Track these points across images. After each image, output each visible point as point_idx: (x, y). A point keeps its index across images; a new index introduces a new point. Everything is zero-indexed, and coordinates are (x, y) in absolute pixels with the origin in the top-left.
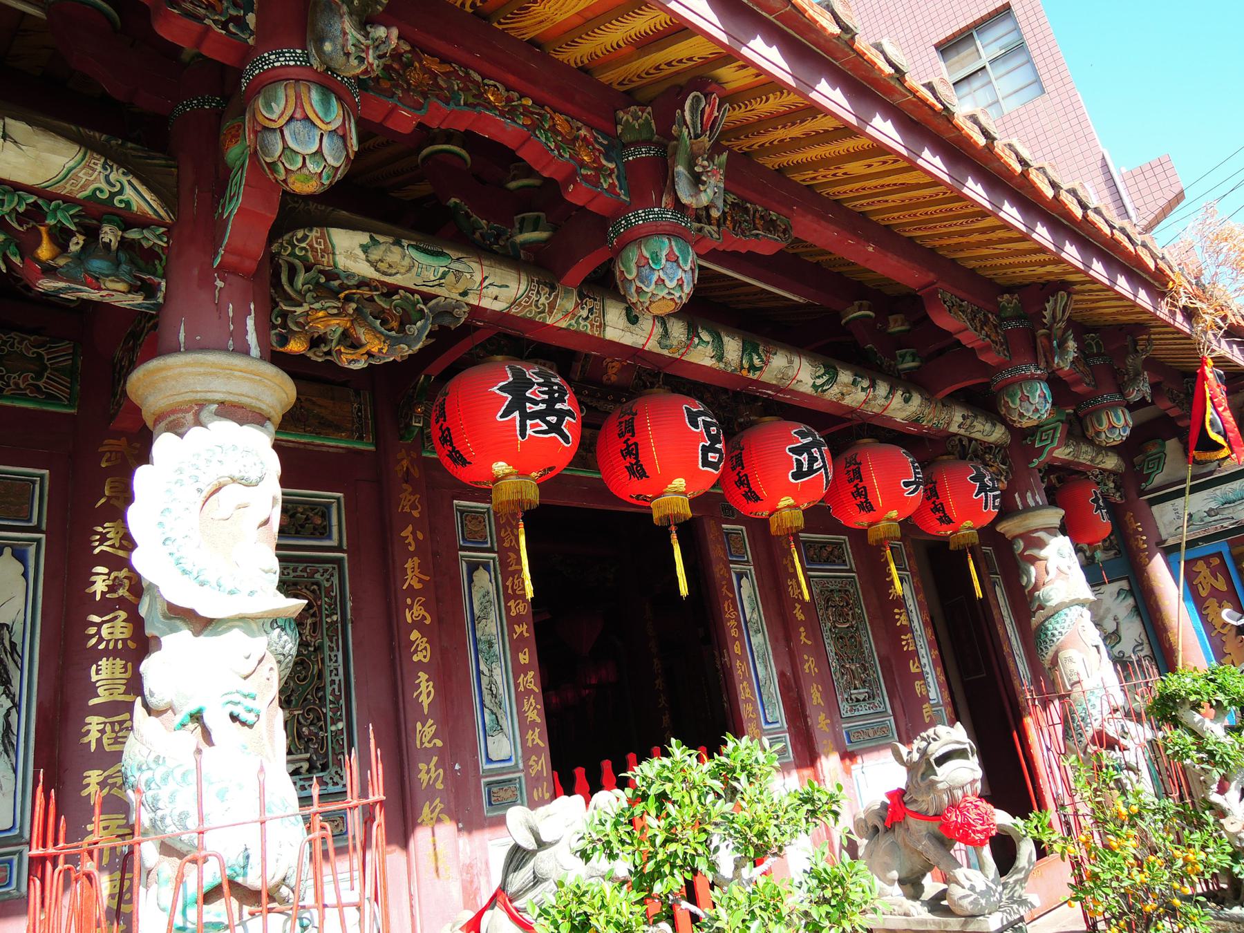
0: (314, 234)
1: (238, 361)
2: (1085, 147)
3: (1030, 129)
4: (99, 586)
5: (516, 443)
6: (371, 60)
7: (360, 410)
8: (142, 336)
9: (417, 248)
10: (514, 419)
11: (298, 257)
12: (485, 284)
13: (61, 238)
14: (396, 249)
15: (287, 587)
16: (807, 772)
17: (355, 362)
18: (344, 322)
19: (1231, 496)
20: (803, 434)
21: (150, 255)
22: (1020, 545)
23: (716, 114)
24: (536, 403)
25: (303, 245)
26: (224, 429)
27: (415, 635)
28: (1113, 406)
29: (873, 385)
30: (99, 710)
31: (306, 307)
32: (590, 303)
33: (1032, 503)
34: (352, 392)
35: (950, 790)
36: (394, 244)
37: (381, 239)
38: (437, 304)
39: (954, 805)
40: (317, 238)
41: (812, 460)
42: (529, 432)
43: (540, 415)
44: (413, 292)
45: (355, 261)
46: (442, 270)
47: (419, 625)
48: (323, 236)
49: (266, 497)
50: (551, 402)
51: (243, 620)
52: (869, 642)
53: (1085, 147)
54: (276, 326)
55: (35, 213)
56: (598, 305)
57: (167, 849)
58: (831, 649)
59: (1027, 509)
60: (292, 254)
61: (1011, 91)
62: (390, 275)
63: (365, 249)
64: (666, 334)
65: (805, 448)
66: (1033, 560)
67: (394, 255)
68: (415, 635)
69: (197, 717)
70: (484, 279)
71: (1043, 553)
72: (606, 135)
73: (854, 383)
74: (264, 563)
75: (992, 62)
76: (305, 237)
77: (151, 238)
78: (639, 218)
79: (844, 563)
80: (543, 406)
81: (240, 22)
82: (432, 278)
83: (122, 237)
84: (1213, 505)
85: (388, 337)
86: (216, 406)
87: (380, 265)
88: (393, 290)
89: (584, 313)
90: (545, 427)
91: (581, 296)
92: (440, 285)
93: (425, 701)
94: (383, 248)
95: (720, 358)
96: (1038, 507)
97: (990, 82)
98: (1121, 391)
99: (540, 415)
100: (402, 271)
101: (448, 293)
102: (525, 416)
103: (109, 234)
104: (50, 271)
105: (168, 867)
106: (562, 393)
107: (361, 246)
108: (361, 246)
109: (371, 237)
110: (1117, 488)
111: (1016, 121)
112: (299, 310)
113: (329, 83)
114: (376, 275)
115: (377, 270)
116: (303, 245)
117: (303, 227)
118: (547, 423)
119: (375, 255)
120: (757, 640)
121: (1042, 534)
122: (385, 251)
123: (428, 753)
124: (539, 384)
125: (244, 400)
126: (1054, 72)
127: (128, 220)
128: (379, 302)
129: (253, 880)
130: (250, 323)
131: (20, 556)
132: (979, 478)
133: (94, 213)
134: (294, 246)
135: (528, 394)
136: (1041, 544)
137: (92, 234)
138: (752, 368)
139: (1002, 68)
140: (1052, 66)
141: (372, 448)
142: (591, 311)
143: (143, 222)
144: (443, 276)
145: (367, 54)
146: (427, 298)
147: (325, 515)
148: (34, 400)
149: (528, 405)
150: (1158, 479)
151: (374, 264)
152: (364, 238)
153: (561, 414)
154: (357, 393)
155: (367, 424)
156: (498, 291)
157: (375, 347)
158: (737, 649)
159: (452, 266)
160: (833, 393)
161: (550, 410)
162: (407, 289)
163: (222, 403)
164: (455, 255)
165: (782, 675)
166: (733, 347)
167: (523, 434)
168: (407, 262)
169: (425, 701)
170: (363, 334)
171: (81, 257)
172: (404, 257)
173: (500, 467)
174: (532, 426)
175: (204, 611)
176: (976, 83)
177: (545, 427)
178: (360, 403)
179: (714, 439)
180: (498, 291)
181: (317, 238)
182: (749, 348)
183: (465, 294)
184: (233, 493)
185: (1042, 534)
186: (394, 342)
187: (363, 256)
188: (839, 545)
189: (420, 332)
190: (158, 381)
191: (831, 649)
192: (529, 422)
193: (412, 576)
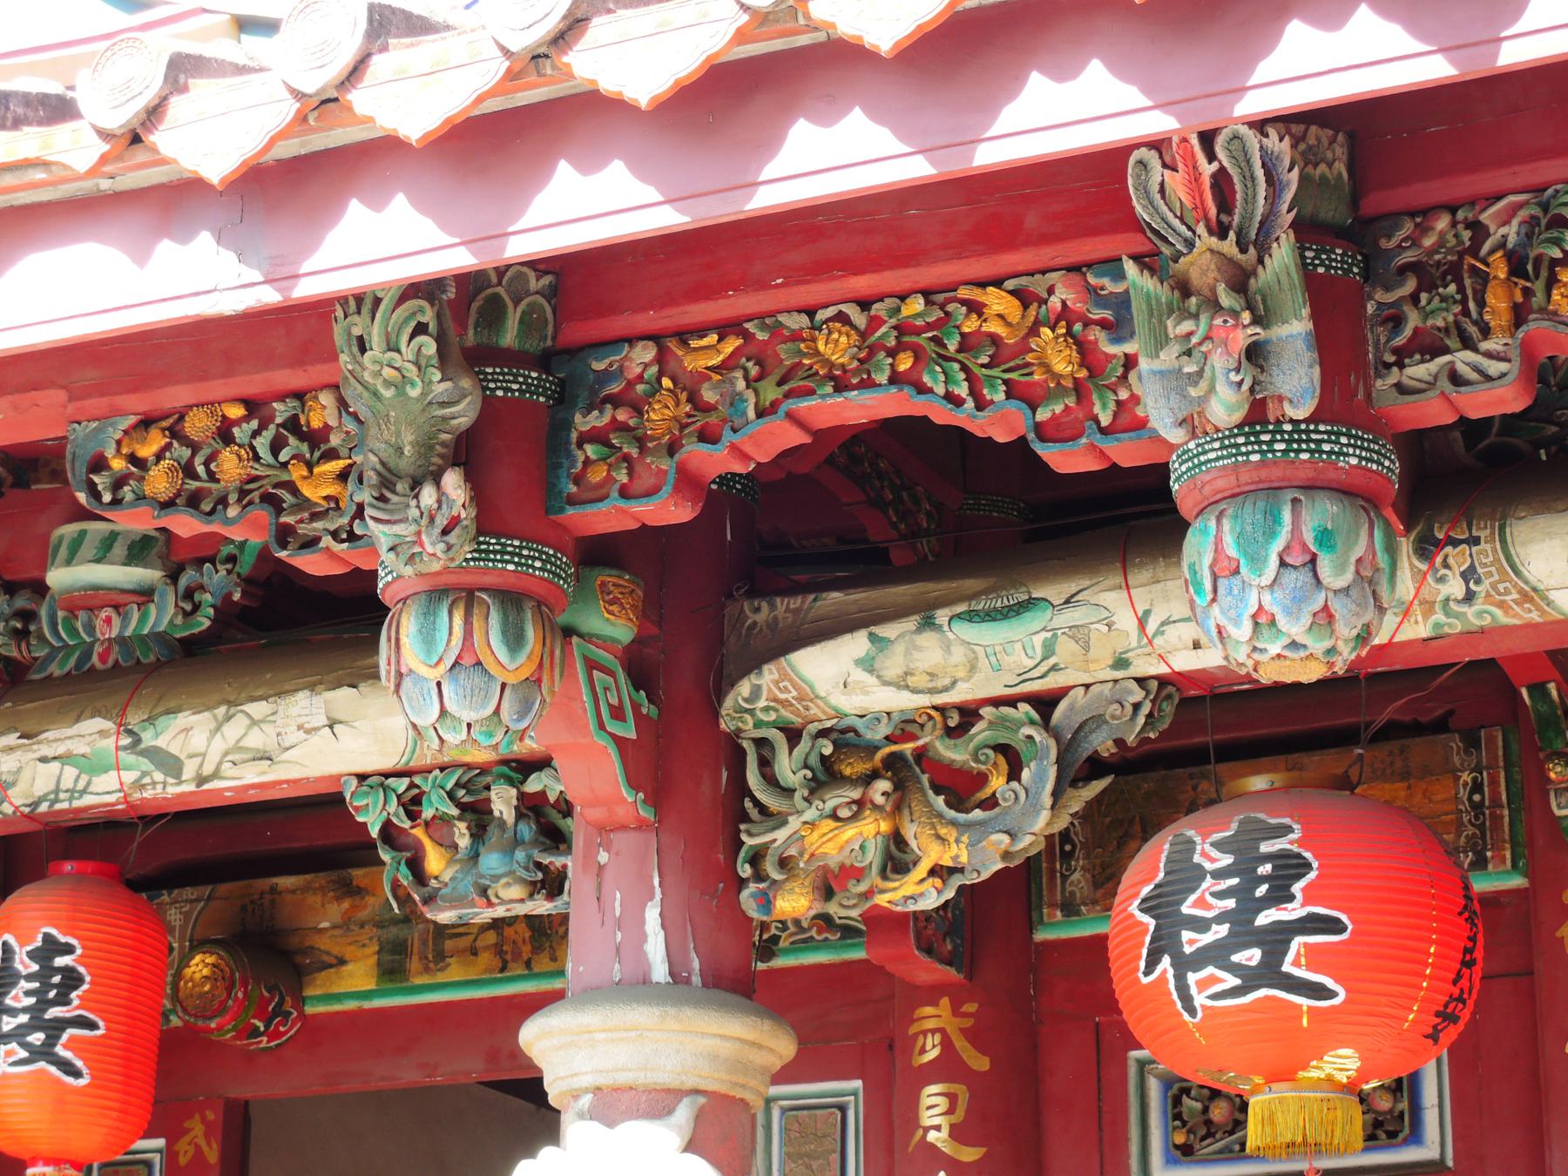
0: (768, 676)
6: (430, 549)
7: (1477, 787)
9: (971, 617)
10: (1162, 979)
11: (768, 724)
12: (1151, 628)
14: (928, 639)
17: (918, 893)
18: (872, 828)
23: (1208, 169)
24: (1201, 925)
25: (762, 703)
31: (794, 823)
32: (1458, 557)
34: (1456, 742)
36: (920, 629)
37: (888, 631)
38: (1071, 708)
40: (776, 683)
42: (1200, 1000)
43: (1216, 954)
44: (1011, 702)
45: (867, 693)
46: (1038, 640)
48: (784, 676)
56: (1486, 552)
60: (758, 724)
62: (946, 689)
63: (868, 664)
70: (1142, 624)
76: (756, 692)
80: (1221, 931)
82: (1030, 663)
83: (522, 796)
85: (969, 826)
86: (590, 1096)
87: (911, 681)
89: (1456, 588)
90: (1232, 981)
91: (1427, 548)
92: (1054, 668)
94: (899, 648)
99: (1216, 954)
100: (961, 674)
102: (1183, 965)
107: (859, 662)
108: (859, 662)
109: (873, 638)
112: (781, 835)
114: (924, 700)
115: (915, 691)
116: (762, 703)
117: (745, 673)
118: (1235, 969)
119: (893, 665)
122: (907, 653)
124: (1219, 875)
125: (623, 1078)
128: (911, 767)
130: (652, 915)
134: (751, 712)
135: (1186, 909)
141: (1517, 881)
142: (1469, 575)
144: (1049, 649)
145: (422, 545)
146: (1045, 703)
148: (825, 945)
149: (1186, 935)
151: (901, 684)
152: (856, 644)
154: (1471, 742)
155: (1496, 820)
157: (953, 853)
159: (1056, 623)
161: (1243, 933)
162: (997, 702)
163: (597, 1090)
164: (1053, 591)
167: (1192, 1011)
168: (958, 655)
172: (947, 647)
174: (1203, 985)
177: (1232, 981)
178: (1478, 769)
181: (776, 683)
183: (1121, 663)
187: (871, 680)
192: (1192, 978)
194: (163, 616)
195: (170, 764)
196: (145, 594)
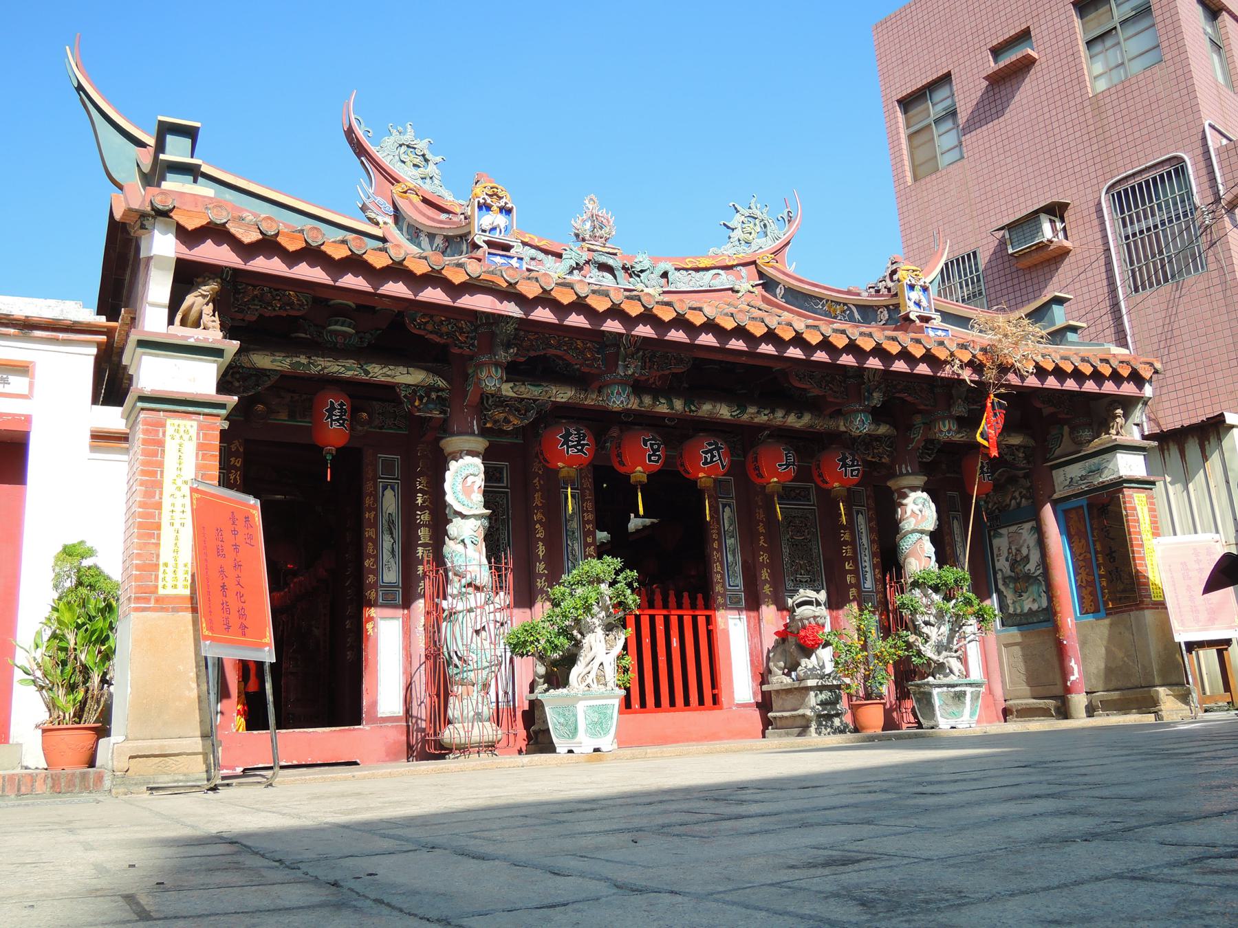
1: (472, 438)
2: (1190, 118)
3: (1145, 96)
4: (420, 501)
5: (569, 452)
8: (445, 429)
13: (421, 399)
15: (486, 507)
16: (753, 614)
19: (1093, 468)
20: (710, 444)
21: (445, 399)
22: (896, 495)
26: (468, 459)
27: (538, 526)
28: (943, 419)
29: (773, 412)
30: (421, 545)
33: (904, 471)
35: (801, 620)
39: (804, 627)
41: (713, 456)
43: (574, 446)
47: (539, 522)
49: (479, 481)
50: (579, 442)
51: (474, 516)
52: (818, 549)
53: (1190, 118)
54: (482, 420)
55: (415, 392)
57: (455, 574)
58: (786, 551)
59: (902, 474)
61: (1137, 53)
64: (641, 402)
65: (710, 451)
66: (901, 505)
67: (523, 389)
68: (538, 526)
69: (463, 541)
71: (905, 502)
72: (598, 343)
73: (758, 412)
74: (478, 498)
75: (1122, 23)
77: (444, 395)
78: (608, 377)
79: (809, 500)
81: (473, 345)
84: (1084, 473)
88: (523, 399)
93: (541, 554)
95: (672, 409)
96: (908, 474)
97: (1119, 43)
98: (949, 407)
99: (574, 446)
101: (544, 398)
103: (434, 395)
104: (419, 410)
105: (456, 579)
106: (584, 436)
110: (1026, 458)
111: (1134, 87)
113: (497, 365)
120: (730, 542)
121: (906, 490)
123: (541, 576)
126: (1173, 40)
127: (439, 389)
129: (478, 583)
131: (393, 489)
132: (843, 460)
133: (430, 389)
136: (905, 496)
137: (429, 397)
138: (691, 411)
139: (1131, 30)
140: (1171, 34)
143: (442, 390)
146: (535, 401)
147: (501, 473)
150: (1058, 452)
153: (583, 445)
156: (563, 395)
158: (715, 545)
160: (745, 417)
161: (579, 444)
165: (744, 563)
166: (678, 404)
169: (541, 554)
170: (511, 418)
171: (426, 404)
173: (560, 464)
175: (465, 513)
176: (1109, 42)
179: (655, 451)
180: (563, 395)
182: (687, 402)
184: (470, 479)
185: (906, 490)
186: (522, 420)
188: (808, 489)
189: (532, 415)
190: (452, 443)
191: (786, 551)
193: (538, 500)
194: (355, 340)
195: (367, 373)
196: (350, 335)
